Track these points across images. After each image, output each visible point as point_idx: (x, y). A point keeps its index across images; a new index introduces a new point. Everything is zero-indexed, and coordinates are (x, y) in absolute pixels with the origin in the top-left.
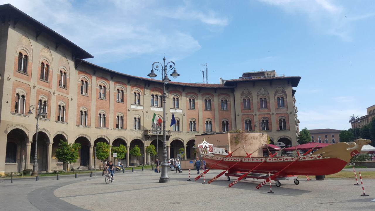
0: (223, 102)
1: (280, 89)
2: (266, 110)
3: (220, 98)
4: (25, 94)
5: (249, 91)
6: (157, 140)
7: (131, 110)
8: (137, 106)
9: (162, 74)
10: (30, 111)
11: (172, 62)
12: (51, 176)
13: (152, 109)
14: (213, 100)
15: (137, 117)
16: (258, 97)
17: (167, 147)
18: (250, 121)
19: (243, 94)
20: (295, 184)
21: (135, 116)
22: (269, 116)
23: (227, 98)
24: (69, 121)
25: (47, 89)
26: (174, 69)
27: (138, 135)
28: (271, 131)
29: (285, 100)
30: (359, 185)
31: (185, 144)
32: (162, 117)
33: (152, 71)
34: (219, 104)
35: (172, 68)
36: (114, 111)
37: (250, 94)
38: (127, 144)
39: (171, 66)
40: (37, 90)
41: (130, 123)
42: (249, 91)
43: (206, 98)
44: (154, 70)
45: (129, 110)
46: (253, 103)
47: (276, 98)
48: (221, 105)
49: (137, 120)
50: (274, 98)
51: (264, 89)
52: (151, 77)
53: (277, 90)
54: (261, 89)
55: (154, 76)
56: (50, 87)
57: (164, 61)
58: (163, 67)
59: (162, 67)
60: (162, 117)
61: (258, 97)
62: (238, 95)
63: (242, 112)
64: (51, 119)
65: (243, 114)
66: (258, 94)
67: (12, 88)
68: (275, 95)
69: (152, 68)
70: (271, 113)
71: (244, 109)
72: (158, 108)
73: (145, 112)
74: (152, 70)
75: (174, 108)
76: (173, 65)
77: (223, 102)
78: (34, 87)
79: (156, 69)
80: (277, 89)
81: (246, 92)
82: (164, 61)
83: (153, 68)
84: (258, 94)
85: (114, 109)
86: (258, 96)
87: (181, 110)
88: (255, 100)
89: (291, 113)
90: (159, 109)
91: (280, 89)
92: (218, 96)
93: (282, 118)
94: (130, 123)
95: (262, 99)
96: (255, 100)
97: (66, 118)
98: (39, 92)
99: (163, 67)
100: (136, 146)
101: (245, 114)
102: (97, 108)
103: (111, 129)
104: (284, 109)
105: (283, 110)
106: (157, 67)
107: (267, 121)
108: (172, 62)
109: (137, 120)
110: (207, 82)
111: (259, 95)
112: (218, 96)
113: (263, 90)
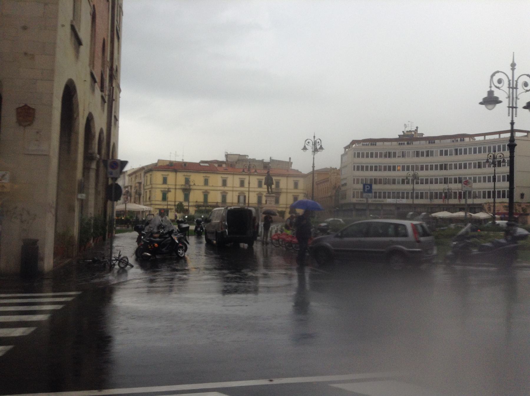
10: (305, 146)
11: (319, 139)
12: (107, 49)
26: (320, 145)
32: (145, 215)
33: (305, 146)
35: (319, 144)
44: (306, 145)
57: (314, 138)
59: (509, 81)
60: (145, 215)
69: (489, 85)
74: (489, 89)
79: (307, 144)
82: (314, 138)
83: (492, 85)
87: (237, 202)
100: (155, 245)
108: (319, 139)
110: (426, 142)
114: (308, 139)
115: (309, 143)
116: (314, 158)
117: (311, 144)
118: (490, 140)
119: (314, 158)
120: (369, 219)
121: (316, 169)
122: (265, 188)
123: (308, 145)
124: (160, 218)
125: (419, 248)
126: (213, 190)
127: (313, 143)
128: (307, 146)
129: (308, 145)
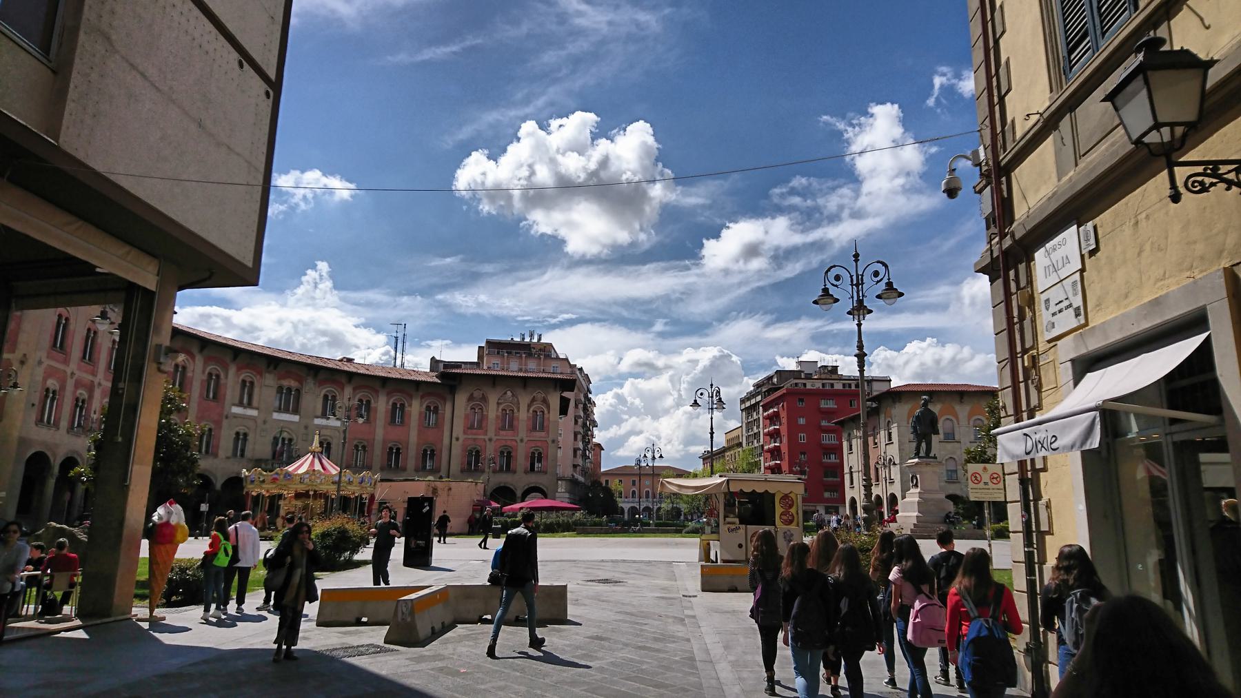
0: (430, 411)
1: (540, 396)
2: (510, 432)
3: (425, 401)
5: (483, 394)
8: (245, 407)
9: (852, 297)
10: (695, 401)
14: (410, 405)
16: (498, 407)
18: (478, 452)
19: (471, 398)
21: (237, 429)
22: (514, 443)
25: (90, 378)
26: (885, 280)
29: (546, 416)
33: (695, 401)
34: (420, 413)
35: (879, 278)
37: (484, 399)
39: (876, 274)
40: (76, 381)
42: (483, 394)
43: (430, 403)
44: (829, 286)
45: (227, 417)
46: (487, 417)
47: (531, 411)
48: (424, 415)
50: (528, 411)
51: (511, 392)
52: (885, 300)
53: (534, 397)
54: (506, 393)
55: (895, 294)
56: (94, 374)
57: (856, 261)
58: (854, 278)
59: (851, 277)
61: (498, 407)
62: (461, 399)
63: (465, 433)
65: (466, 436)
66: (500, 401)
68: (529, 406)
70: (518, 439)
71: (469, 427)
72: (288, 415)
73: (260, 421)
74: (823, 287)
75: (241, 404)
76: (882, 269)
77: (430, 411)
78: (73, 374)
79: (835, 283)
80: (535, 394)
81: (477, 394)
82: (856, 261)
84: (500, 401)
86: (498, 404)
88: (493, 412)
89: (553, 441)
90: (292, 416)
91: (539, 395)
92: (422, 397)
93: (537, 450)
95: (536, 412)
96: (493, 412)
98: (78, 384)
99: (854, 278)
101: (470, 437)
104: (543, 434)
105: (539, 435)
106: (837, 278)
107: (509, 453)
108: (878, 262)
109: (241, 439)
111: (501, 404)
112: (422, 397)
113: (509, 393)
114: (835, 266)
115: (702, 394)
116: (712, 418)
117: (706, 396)
118: (1019, 388)
119: (712, 418)
120: (833, 555)
121: (28, 614)
122: (1205, 464)
123: (836, 286)
124: (911, 178)
125: (24, 121)
126: (980, 183)
127: (852, 281)
128: (699, 401)
129: (836, 286)
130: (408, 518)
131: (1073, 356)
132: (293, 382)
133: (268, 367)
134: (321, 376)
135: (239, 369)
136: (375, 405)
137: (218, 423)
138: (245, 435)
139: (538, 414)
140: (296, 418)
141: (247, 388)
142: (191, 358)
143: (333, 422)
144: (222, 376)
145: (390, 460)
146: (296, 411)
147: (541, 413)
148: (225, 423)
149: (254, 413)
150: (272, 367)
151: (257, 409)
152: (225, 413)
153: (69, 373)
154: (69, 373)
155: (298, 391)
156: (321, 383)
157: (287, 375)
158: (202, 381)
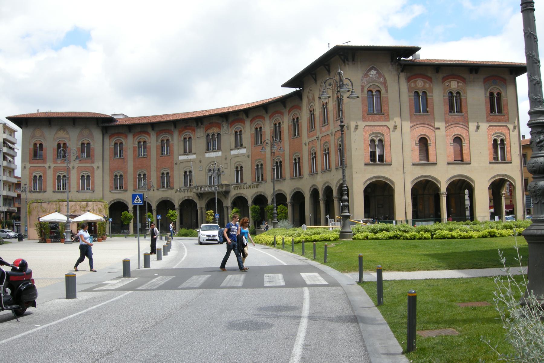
4: (42, 174)
6: (215, 198)
7: (178, 163)
13: (207, 155)
15: (188, 171)
17: (227, 208)
20: (86, 259)
21: (185, 170)
23: (145, 138)
24: (95, 189)
27: (191, 195)
28: (126, 191)
30: (95, 271)
31: (177, 206)
36: (157, 168)
38: (174, 206)
41: (178, 180)
49: (188, 174)
64: (72, 190)
67: (28, 173)
75: (185, 153)
85: (157, 166)
94: (178, 180)
97: (337, 158)
102: (135, 168)
103: (154, 190)
109: (188, 174)
130: (18, 268)
131: (418, 299)
132: (215, 129)
133: (197, 125)
134: (231, 119)
135: (180, 132)
136: (264, 130)
137: (172, 169)
138: (190, 172)
139: (374, 93)
140: (219, 154)
141: (187, 141)
142: (148, 135)
143: (243, 151)
144: (170, 140)
145: (496, 152)
146: (219, 149)
147: (378, 93)
148: (176, 167)
149: (193, 157)
150: (200, 124)
151: (195, 154)
152: (175, 162)
153: (47, 167)
154: (47, 167)
155: (219, 134)
156: (231, 124)
157: (211, 125)
158: (157, 146)
